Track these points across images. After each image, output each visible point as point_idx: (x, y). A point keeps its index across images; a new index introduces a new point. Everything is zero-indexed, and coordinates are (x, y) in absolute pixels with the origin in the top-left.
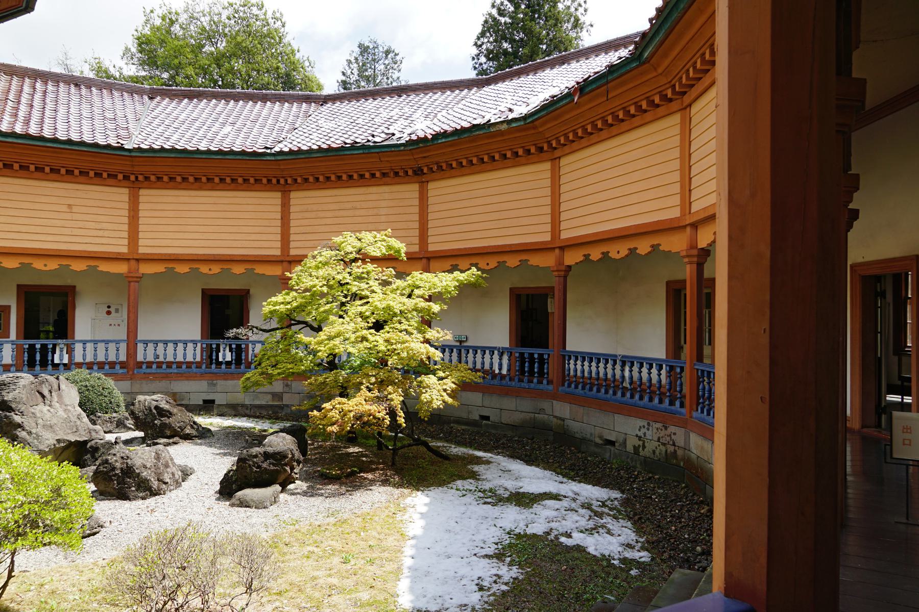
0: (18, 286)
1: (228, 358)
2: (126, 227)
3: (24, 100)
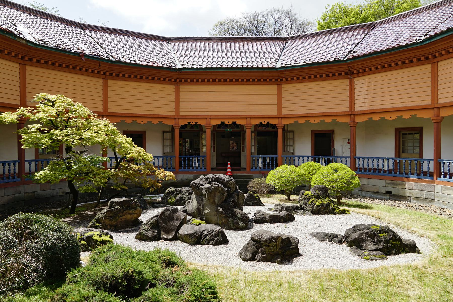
0: (312, 131)
3: (216, 53)
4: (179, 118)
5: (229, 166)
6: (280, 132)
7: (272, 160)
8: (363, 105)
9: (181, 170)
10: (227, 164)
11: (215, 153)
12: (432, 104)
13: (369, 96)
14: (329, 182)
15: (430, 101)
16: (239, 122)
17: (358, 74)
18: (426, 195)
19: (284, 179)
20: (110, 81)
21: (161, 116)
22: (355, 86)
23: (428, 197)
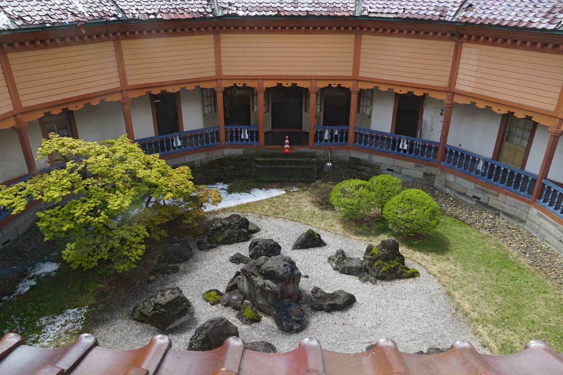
1: (405, 148)
2: (223, 64)
4: (221, 79)
5: (287, 141)
6: (354, 98)
7: (341, 133)
8: (467, 83)
9: (227, 143)
10: (285, 139)
11: (270, 114)
12: (555, 111)
13: (478, 75)
14: (403, 220)
15: (555, 107)
16: (300, 84)
17: (469, 40)
18: (517, 212)
19: (350, 207)
20: (123, 42)
21: (198, 80)
22: (462, 54)
23: (519, 216)
